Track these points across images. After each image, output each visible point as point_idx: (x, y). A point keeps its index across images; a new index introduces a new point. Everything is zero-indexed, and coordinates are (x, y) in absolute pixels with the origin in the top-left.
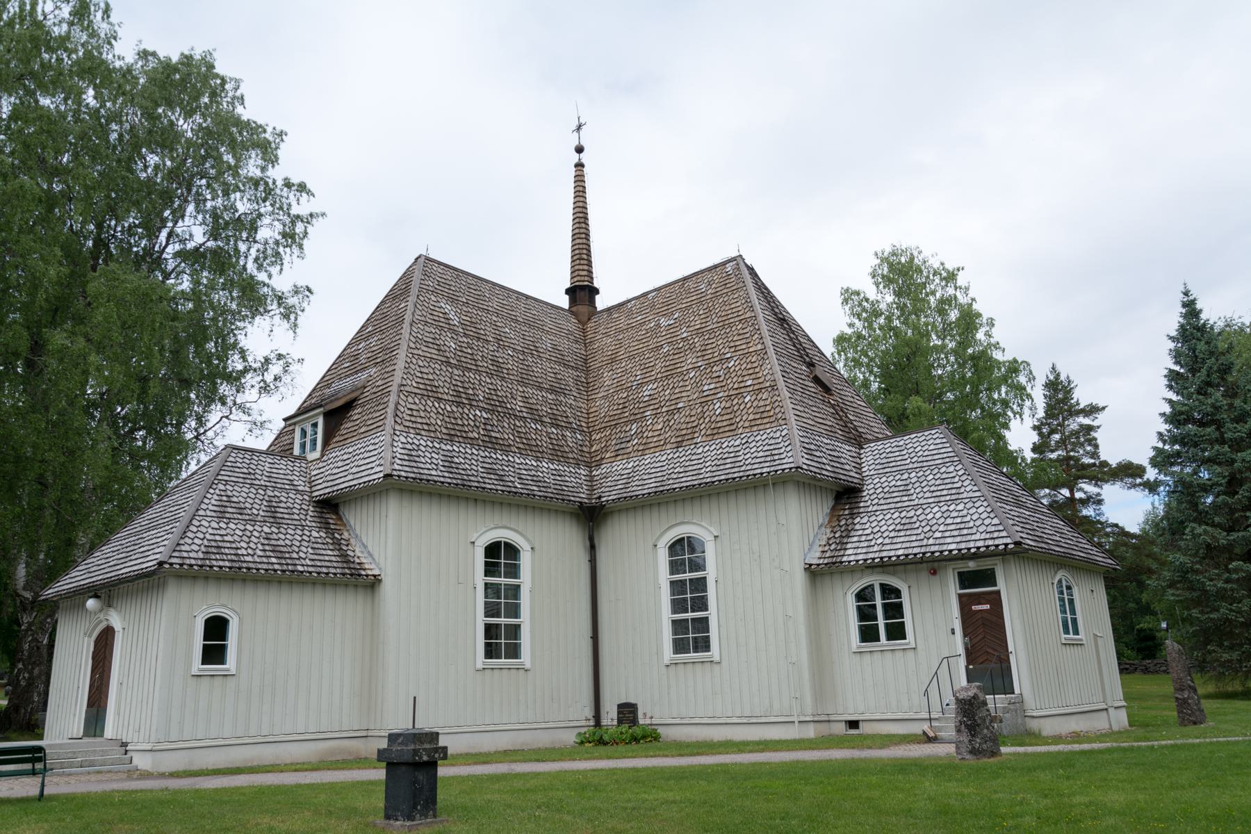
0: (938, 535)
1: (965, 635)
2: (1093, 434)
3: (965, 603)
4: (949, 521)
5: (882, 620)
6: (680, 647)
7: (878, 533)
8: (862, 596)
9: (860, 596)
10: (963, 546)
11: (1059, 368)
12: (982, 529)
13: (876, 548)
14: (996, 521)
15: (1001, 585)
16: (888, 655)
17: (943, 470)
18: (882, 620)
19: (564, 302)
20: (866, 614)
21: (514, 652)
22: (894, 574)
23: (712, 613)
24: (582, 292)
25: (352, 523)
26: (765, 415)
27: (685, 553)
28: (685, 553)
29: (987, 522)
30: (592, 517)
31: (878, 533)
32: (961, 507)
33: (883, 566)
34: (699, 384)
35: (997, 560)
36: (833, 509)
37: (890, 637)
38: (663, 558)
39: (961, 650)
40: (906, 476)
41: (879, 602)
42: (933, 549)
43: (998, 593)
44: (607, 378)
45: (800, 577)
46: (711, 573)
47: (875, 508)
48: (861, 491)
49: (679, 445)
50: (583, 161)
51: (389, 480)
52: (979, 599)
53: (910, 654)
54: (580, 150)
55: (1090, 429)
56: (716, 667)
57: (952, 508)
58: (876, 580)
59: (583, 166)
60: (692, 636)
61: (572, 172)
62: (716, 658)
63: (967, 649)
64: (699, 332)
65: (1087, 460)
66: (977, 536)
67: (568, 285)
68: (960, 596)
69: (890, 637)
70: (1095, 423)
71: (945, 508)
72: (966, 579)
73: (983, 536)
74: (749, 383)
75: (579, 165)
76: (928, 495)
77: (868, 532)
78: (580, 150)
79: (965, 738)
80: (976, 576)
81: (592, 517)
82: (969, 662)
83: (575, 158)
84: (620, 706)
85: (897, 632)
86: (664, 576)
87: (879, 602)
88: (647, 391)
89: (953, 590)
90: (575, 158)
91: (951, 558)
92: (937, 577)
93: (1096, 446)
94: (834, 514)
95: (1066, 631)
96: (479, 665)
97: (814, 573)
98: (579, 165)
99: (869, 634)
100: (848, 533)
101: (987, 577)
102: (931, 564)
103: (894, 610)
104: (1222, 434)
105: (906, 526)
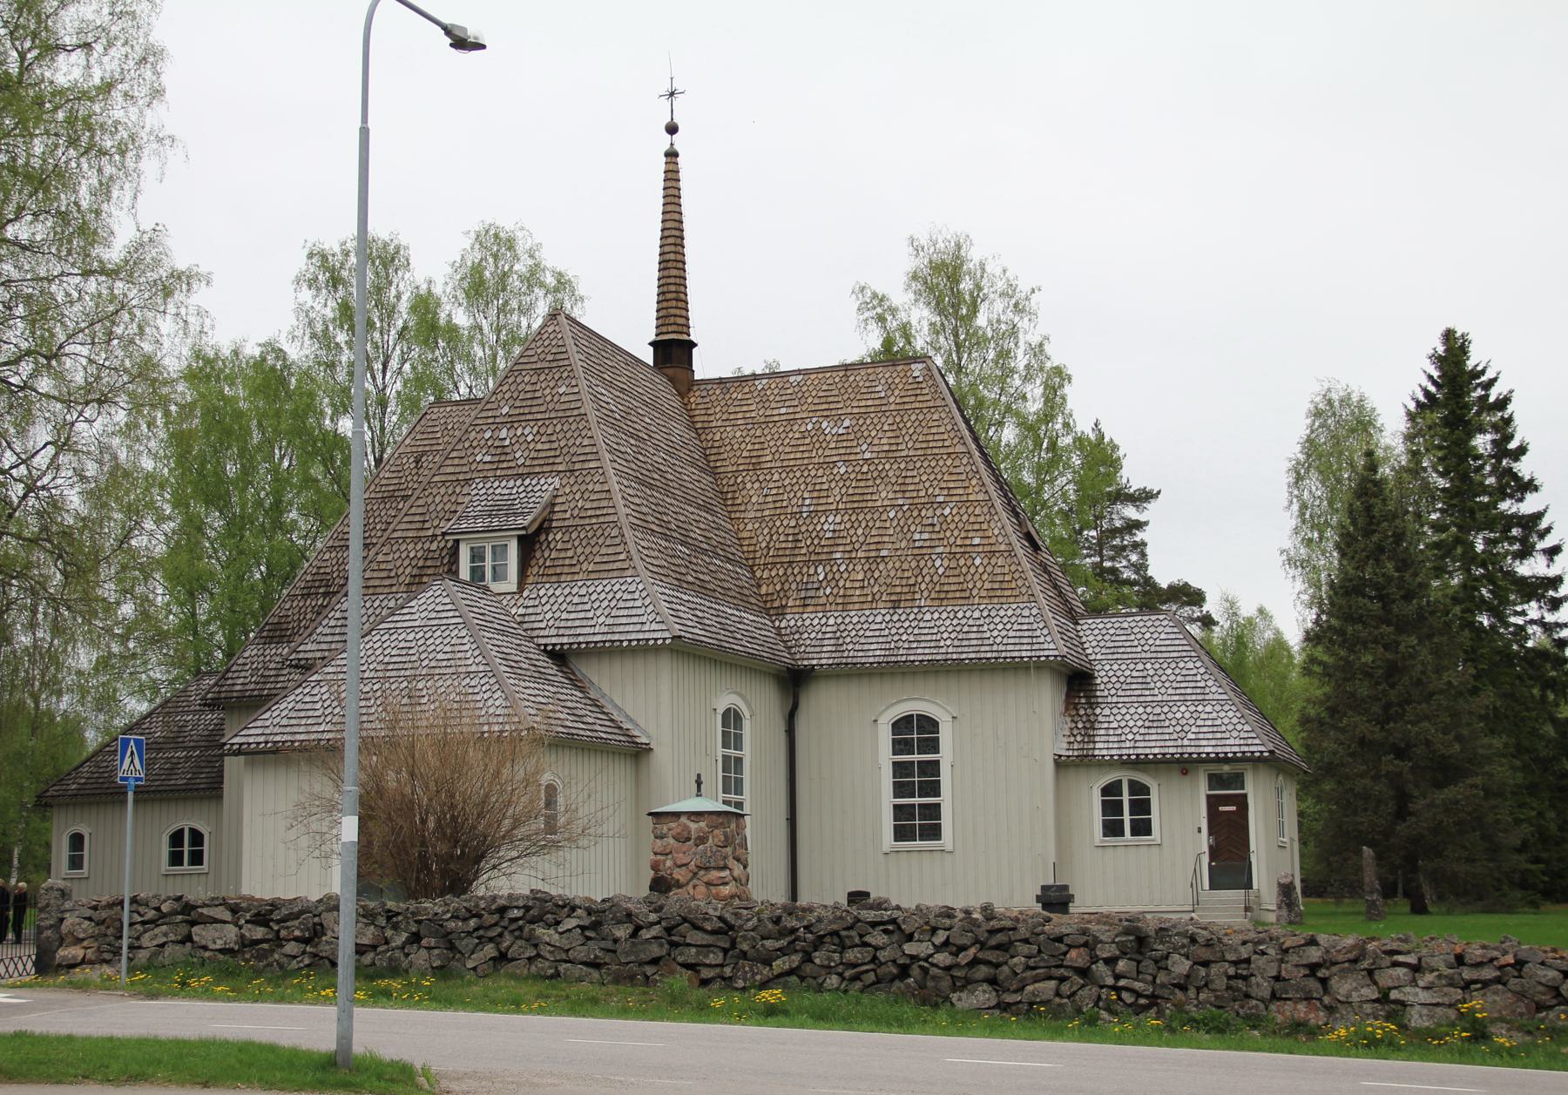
0: (1191, 736)
1: (1210, 833)
2: (1140, 536)
3: (1213, 802)
4: (1199, 722)
5: (1126, 814)
6: (901, 834)
7: (1123, 728)
8: (1111, 790)
9: (1106, 791)
10: (1219, 750)
11: (1103, 427)
12: (1235, 734)
13: (1128, 744)
14: (1247, 728)
15: (1250, 789)
16: (1133, 850)
17: (1181, 665)
18: (1126, 814)
19: (648, 356)
20: (1111, 807)
21: (934, 832)
22: (1144, 771)
23: (946, 799)
24: (674, 351)
25: (595, 680)
26: (1005, 585)
27: (916, 734)
28: (916, 734)
29: (1239, 727)
30: (794, 681)
31: (1123, 728)
32: (1209, 709)
33: (1139, 763)
34: (904, 530)
35: (1248, 766)
36: (1068, 696)
37: (1134, 832)
38: (885, 737)
39: (1206, 849)
40: (1140, 666)
41: (1126, 798)
42: (1190, 750)
43: (1245, 796)
44: (752, 492)
45: (1050, 765)
46: (945, 756)
47: (1115, 699)
48: (1092, 677)
49: (895, 605)
50: (677, 147)
51: (677, 641)
52: (1227, 800)
53: (1155, 850)
54: (672, 129)
55: (1139, 525)
56: (948, 857)
57: (1200, 708)
58: (1125, 776)
59: (676, 155)
60: (918, 822)
61: (661, 163)
62: (949, 847)
63: (1211, 847)
64: (890, 455)
65: (1128, 574)
66: (1231, 742)
67: (652, 337)
68: (1209, 797)
69: (1134, 832)
70: (1142, 518)
71: (1192, 708)
72: (1215, 781)
73: (1237, 742)
74: (977, 541)
75: (672, 155)
76: (1170, 691)
77: (1115, 725)
78: (672, 129)
79: (1284, 912)
80: (1225, 779)
81: (794, 681)
82: (1212, 859)
83: (665, 141)
84: (850, 894)
85: (1142, 828)
86: (886, 757)
87: (1126, 798)
88: (829, 524)
89: (1203, 790)
90: (665, 141)
91: (1208, 760)
92: (1187, 779)
93: (1143, 555)
94: (1070, 704)
95: (197, 837)
96: (886, 848)
97: (1061, 764)
98: (672, 155)
99: (1113, 829)
100: (1091, 725)
101: (1238, 780)
102: (1184, 765)
103: (1141, 807)
104: (1389, 612)
105: (1154, 723)
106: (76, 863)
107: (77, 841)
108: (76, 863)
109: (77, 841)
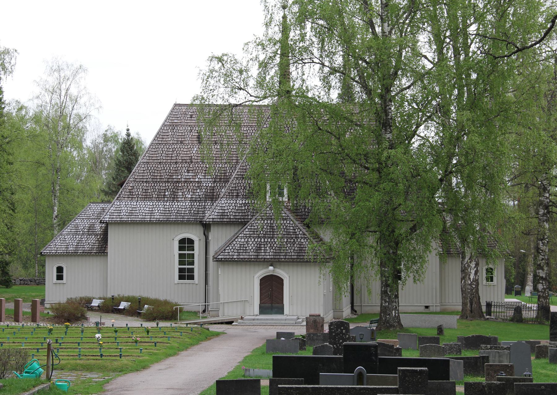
96: (176, 282)
106: (60, 277)
107: (60, 270)
108: (60, 277)
109: (60, 270)
